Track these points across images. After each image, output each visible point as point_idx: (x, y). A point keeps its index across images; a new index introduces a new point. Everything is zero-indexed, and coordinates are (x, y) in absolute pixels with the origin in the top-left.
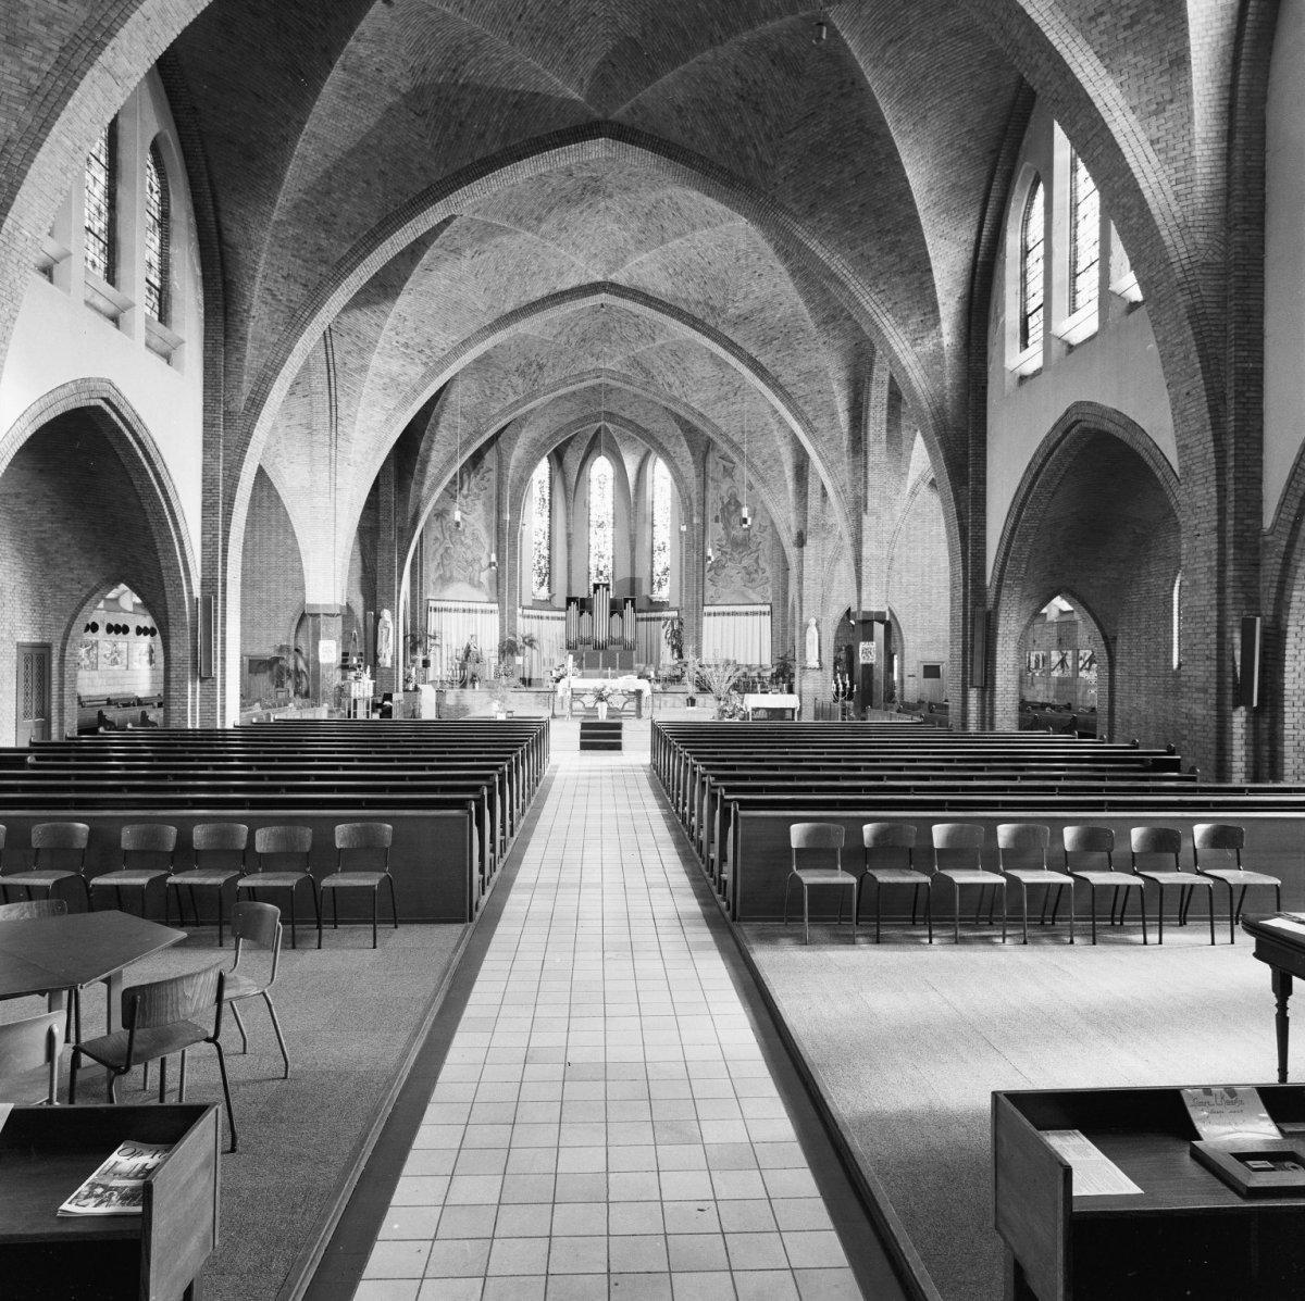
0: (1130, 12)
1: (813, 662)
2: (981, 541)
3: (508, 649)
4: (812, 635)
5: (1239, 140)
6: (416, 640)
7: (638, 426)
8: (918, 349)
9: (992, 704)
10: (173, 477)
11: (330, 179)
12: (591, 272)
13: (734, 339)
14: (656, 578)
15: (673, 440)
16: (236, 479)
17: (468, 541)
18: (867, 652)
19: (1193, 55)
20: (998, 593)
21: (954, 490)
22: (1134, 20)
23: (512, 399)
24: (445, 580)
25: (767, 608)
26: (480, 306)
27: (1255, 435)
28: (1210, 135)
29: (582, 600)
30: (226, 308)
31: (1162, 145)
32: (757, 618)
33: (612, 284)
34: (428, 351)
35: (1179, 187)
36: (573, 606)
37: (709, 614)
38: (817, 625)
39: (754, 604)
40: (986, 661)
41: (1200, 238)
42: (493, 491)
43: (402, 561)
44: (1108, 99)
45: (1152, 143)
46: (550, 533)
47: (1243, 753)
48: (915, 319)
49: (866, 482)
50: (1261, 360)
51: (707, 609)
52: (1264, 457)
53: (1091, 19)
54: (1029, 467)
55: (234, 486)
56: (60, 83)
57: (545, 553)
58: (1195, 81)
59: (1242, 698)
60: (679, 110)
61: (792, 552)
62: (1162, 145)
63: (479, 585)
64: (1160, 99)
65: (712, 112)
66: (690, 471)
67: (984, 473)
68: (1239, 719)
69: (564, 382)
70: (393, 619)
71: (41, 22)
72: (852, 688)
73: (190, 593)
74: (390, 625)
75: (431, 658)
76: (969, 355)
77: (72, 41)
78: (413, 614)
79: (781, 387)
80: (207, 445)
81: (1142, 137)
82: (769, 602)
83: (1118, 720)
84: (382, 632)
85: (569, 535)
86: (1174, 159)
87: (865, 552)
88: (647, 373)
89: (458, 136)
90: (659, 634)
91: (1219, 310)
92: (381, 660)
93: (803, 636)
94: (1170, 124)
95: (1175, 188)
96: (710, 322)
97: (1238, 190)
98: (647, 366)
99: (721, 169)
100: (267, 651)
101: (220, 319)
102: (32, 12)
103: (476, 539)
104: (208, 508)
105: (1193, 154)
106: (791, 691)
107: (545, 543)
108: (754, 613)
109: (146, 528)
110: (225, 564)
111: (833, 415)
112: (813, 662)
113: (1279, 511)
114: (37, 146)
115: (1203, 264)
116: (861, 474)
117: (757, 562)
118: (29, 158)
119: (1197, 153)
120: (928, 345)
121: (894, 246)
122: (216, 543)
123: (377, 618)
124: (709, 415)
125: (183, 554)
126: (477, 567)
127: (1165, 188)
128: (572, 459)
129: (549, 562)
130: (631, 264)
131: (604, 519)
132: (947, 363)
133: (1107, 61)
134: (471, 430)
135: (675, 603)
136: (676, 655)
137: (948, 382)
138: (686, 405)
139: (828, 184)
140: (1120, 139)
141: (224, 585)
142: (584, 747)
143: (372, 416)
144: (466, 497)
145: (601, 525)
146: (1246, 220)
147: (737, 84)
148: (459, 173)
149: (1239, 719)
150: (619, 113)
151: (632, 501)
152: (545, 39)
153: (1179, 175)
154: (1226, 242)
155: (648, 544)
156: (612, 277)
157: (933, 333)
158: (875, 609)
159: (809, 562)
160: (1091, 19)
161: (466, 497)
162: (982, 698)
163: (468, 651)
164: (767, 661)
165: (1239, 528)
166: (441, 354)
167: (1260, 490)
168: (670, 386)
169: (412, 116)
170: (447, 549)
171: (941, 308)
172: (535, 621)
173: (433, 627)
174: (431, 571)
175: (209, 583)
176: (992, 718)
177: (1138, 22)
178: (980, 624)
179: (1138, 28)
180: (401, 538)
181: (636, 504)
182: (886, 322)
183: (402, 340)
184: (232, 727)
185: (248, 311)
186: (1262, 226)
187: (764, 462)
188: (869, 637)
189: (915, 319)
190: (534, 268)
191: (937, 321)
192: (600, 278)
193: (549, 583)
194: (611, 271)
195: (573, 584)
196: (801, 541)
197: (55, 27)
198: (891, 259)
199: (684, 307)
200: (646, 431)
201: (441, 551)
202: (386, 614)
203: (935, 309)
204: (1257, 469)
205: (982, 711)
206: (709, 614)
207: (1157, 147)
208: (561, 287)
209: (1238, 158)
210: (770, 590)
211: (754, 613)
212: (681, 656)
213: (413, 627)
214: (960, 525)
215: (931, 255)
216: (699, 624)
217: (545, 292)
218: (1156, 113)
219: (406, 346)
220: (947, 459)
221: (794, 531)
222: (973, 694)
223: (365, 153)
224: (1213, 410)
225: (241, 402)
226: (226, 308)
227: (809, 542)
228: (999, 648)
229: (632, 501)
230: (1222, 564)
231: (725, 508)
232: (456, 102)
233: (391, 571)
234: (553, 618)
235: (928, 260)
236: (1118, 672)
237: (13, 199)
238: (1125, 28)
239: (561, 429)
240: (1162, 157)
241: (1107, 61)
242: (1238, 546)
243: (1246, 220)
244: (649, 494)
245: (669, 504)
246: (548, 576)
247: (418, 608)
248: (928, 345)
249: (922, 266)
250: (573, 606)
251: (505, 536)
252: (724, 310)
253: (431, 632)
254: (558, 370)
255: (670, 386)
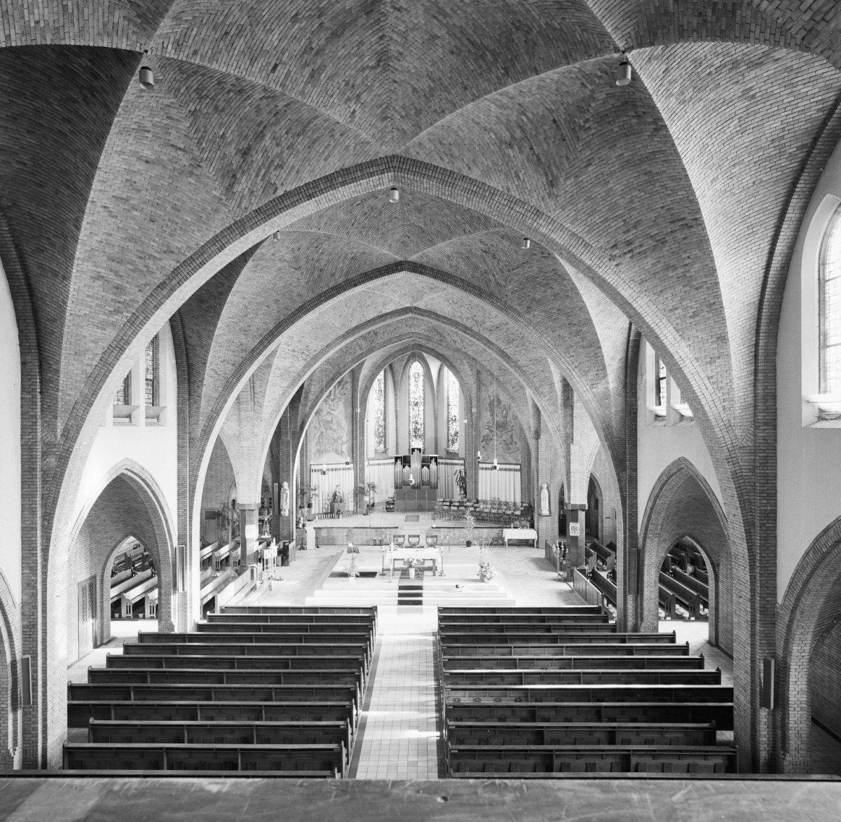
0: (693, 310)
1: (545, 511)
2: (634, 506)
3: (359, 492)
4: (545, 494)
5: (760, 376)
6: (304, 493)
7: (437, 352)
8: (594, 390)
9: (642, 605)
10: (162, 489)
11: (247, 308)
12: (402, 302)
13: (490, 339)
14: (451, 438)
15: (459, 361)
16: (196, 476)
17: (335, 427)
18: (575, 528)
19: (730, 336)
20: (645, 540)
21: (618, 475)
22: (695, 315)
23: (359, 352)
24: (320, 452)
25: (518, 467)
26: (337, 325)
27: (772, 555)
28: (743, 374)
29: (405, 457)
30: (189, 379)
31: (714, 380)
32: (512, 473)
33: (415, 308)
34: (307, 353)
35: (726, 403)
36: (399, 462)
37: (483, 469)
38: (547, 488)
39: (510, 464)
40: (638, 581)
41: (738, 432)
42: (349, 395)
43: (295, 452)
44: (681, 354)
45: (709, 378)
46: (385, 410)
47: (766, 733)
48: (591, 375)
49: (572, 425)
50: (776, 505)
51: (481, 465)
52: (778, 562)
53: (671, 311)
54: (659, 478)
55: (195, 480)
56: (102, 371)
57: (382, 423)
58: (732, 348)
59: (765, 703)
60: (448, 257)
61: (532, 442)
62: (714, 380)
63: (341, 453)
64: (712, 356)
65: (468, 258)
66: (471, 380)
67: (636, 465)
68: (763, 714)
69: (390, 341)
70: (289, 487)
71: (93, 342)
72: (565, 551)
73: (172, 546)
74: (288, 492)
75: (313, 502)
76: (626, 393)
77: (108, 348)
78: (302, 474)
79: (519, 367)
80: (180, 459)
81: (703, 375)
82: (520, 462)
83: (721, 616)
84: (283, 496)
85: (396, 411)
86: (722, 388)
87: (572, 468)
88: (441, 335)
89: (319, 277)
90: (452, 480)
91: (750, 474)
92: (282, 513)
93: (539, 494)
94: (719, 369)
95: (723, 404)
96: (476, 329)
97: (761, 406)
98: (440, 331)
99: (474, 287)
100: (216, 506)
101: (186, 386)
102: (88, 339)
103: (339, 425)
104: (181, 494)
105: (733, 387)
106: (532, 526)
107: (382, 418)
108: (510, 470)
109: (147, 512)
110: (191, 525)
111: (552, 385)
112: (545, 511)
113: (786, 596)
114: (90, 404)
115: (740, 447)
116: (569, 419)
117: (511, 437)
118: (86, 412)
119: (735, 386)
120: (600, 388)
121: (578, 333)
122: (185, 514)
123: (280, 487)
124: (479, 359)
125: (168, 526)
126: (340, 442)
127: (717, 404)
128: (398, 368)
129: (385, 429)
130: (426, 298)
131: (418, 400)
132: (612, 399)
133: (681, 333)
134: (334, 371)
135: (462, 455)
136: (462, 492)
137: (613, 409)
138: (465, 353)
139: (538, 297)
140: (689, 377)
141: (191, 537)
142: (401, 603)
143: (274, 392)
144: (333, 400)
145: (416, 404)
146: (765, 424)
147: (482, 246)
148: (320, 296)
149: (763, 714)
150: (413, 258)
151: (434, 389)
152: (368, 231)
153: (725, 397)
154: (755, 435)
155: (445, 418)
156: (415, 305)
157: (604, 381)
158: (578, 503)
159: (542, 449)
160: (671, 311)
161: (333, 400)
162: (636, 600)
163: (335, 495)
164: (518, 500)
165: (763, 602)
166: (315, 353)
167: (775, 580)
168: (455, 342)
169: (293, 270)
170: (322, 433)
171: (608, 368)
172: (376, 467)
173: (314, 483)
174: (312, 447)
175: (182, 538)
176: (642, 614)
177: (698, 315)
178: (634, 558)
179: (697, 319)
180: (293, 439)
181: (438, 391)
182: (575, 374)
183: (291, 348)
184: (190, 630)
185: (202, 381)
186: (775, 427)
187: (513, 388)
188: (576, 520)
189: (591, 375)
190: (369, 302)
191: (605, 376)
192: (408, 305)
193: (385, 442)
194: (415, 301)
195: (399, 441)
196: (537, 435)
197: (100, 343)
198: (577, 339)
199: (459, 320)
200: (442, 355)
201: (319, 434)
202: (285, 484)
203: (604, 368)
204: (774, 569)
205: (636, 609)
206: (483, 469)
207: (712, 381)
208: (384, 311)
209: (760, 387)
210: (520, 456)
211: (510, 470)
212: (465, 493)
213: (302, 483)
214: (622, 496)
215: (600, 339)
216: (476, 474)
217: (376, 315)
218: (710, 363)
219: (294, 351)
220: (613, 456)
221: (533, 429)
222: (630, 598)
223: (266, 292)
224: (748, 532)
225: (198, 432)
226: (189, 379)
227: (542, 437)
228: (645, 573)
229: (434, 389)
230: (753, 621)
231: (491, 404)
232: (318, 260)
233: (288, 458)
234: (387, 464)
235: (598, 342)
236: (720, 585)
237: (79, 434)
238: (691, 317)
239: (390, 356)
240: (715, 386)
241: (681, 333)
242: (762, 613)
243: (765, 424)
244: (445, 385)
245: (458, 392)
246: (383, 437)
247: (305, 471)
248: (600, 388)
249: (595, 345)
250: (399, 462)
251: (356, 422)
252: (484, 322)
253: (313, 487)
254: (386, 335)
255: (455, 342)
